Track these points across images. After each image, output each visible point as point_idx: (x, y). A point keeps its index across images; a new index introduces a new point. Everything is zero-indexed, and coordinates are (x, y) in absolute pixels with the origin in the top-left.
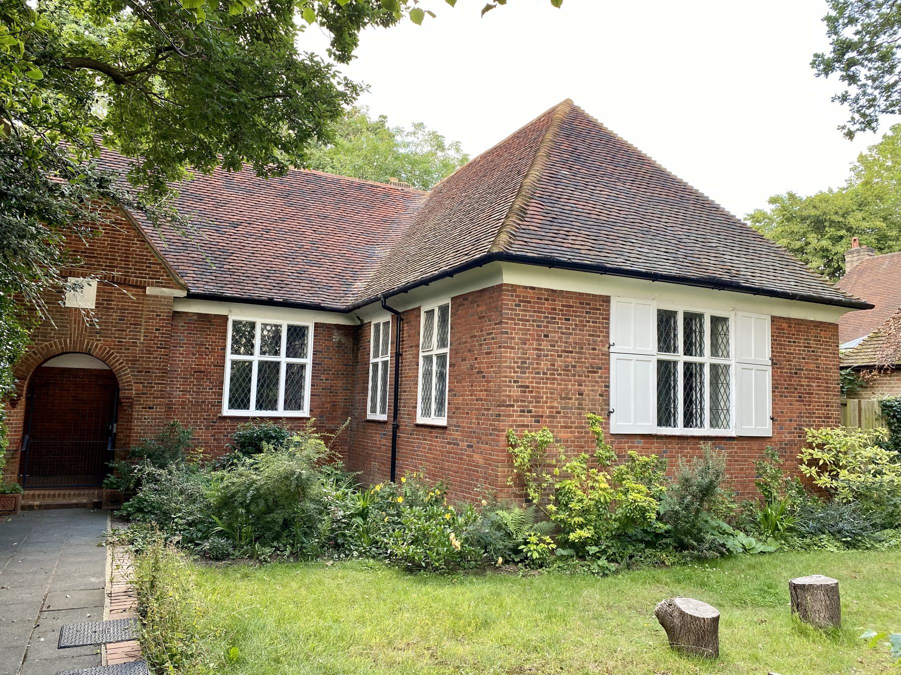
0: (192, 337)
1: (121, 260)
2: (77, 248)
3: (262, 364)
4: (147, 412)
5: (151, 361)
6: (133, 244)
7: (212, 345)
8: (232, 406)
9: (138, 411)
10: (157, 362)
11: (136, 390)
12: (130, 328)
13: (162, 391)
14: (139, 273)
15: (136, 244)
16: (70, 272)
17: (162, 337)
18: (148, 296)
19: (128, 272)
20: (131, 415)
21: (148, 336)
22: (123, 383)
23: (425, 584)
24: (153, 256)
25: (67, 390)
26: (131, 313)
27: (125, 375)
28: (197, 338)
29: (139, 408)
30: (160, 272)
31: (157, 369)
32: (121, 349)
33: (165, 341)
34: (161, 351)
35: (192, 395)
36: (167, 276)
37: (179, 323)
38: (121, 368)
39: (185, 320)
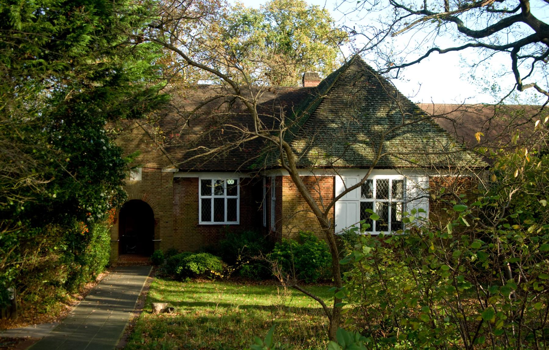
3: (216, 200)
8: (203, 220)
23: (175, 319)
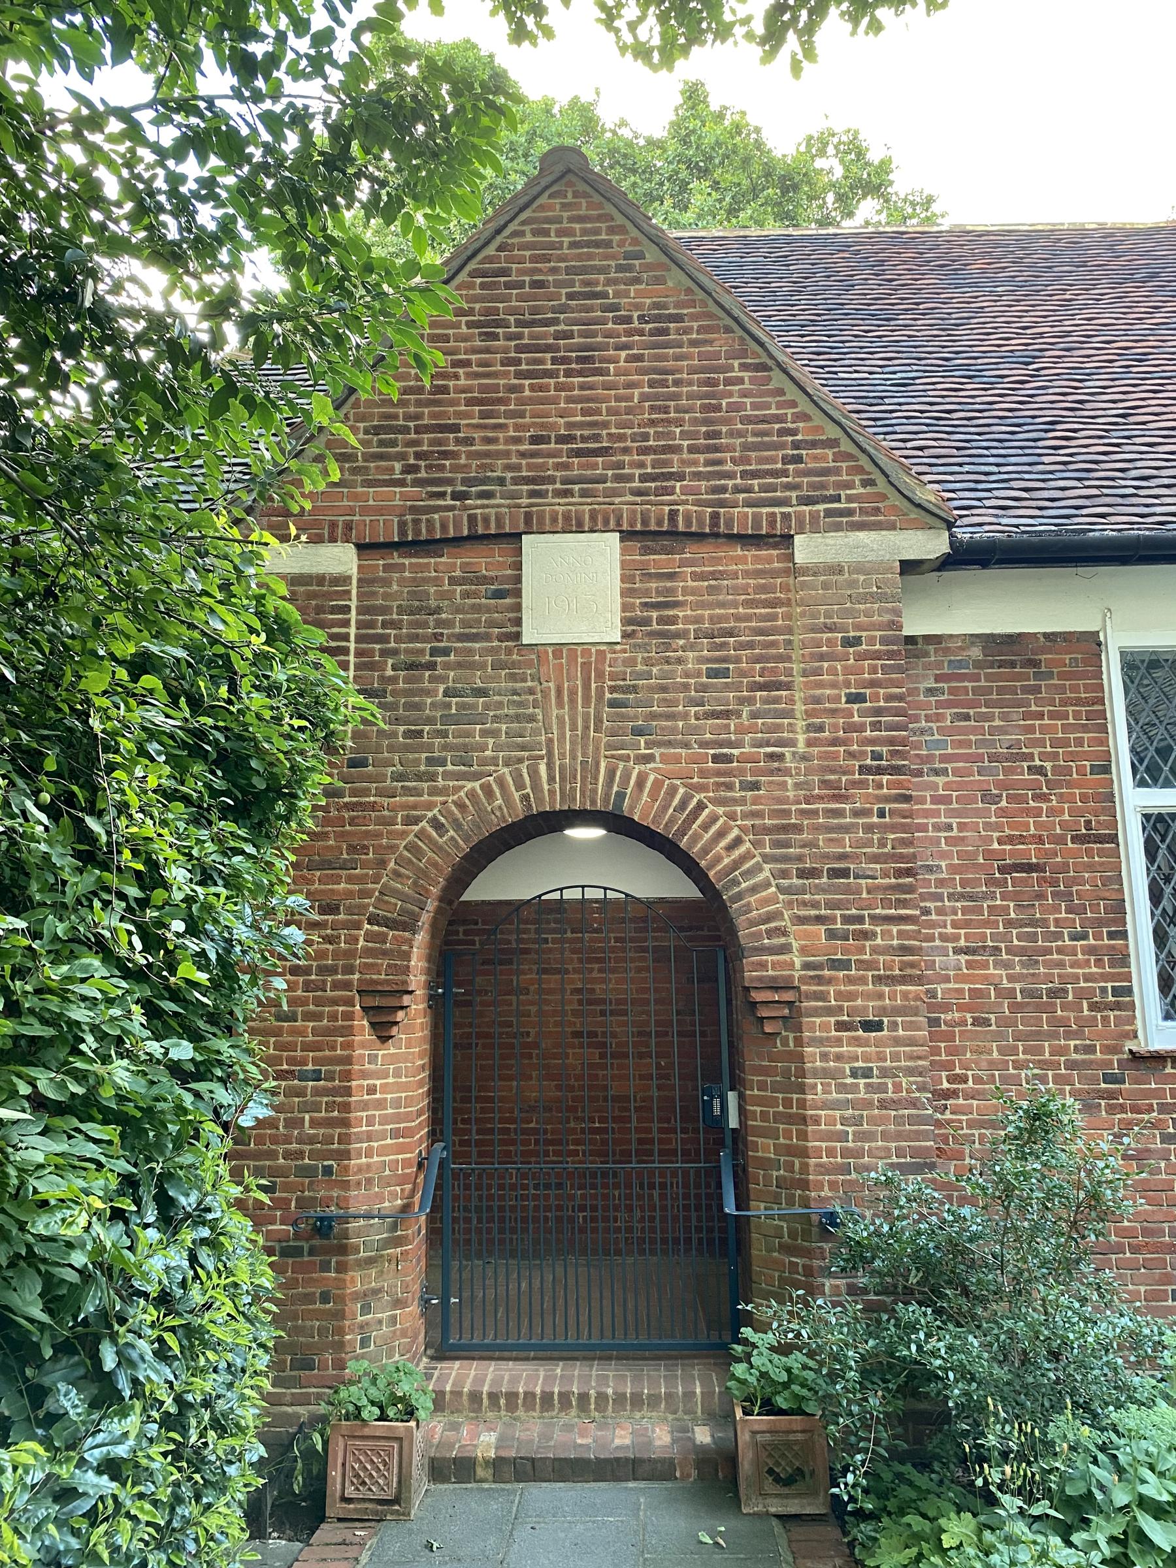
0: (974, 730)
1: (692, 449)
2: (543, 426)
4: (857, 1042)
5: (846, 829)
6: (728, 382)
7: (1054, 757)
9: (821, 1042)
10: (869, 828)
11: (803, 950)
12: (750, 701)
13: (905, 950)
14: (764, 489)
15: (741, 381)
16: (528, 517)
17: (876, 726)
18: (804, 571)
19: (724, 489)
20: (801, 1058)
21: (821, 729)
22: (753, 923)
24: (805, 417)
25: (558, 971)
26: (750, 645)
27: (754, 890)
28: (993, 731)
29: (824, 1027)
30: (837, 471)
31: (875, 859)
32: (729, 787)
33: (891, 742)
34: (880, 786)
35: (1007, 965)
36: (865, 483)
37: (917, 679)
38: (736, 865)
39: (939, 665)
